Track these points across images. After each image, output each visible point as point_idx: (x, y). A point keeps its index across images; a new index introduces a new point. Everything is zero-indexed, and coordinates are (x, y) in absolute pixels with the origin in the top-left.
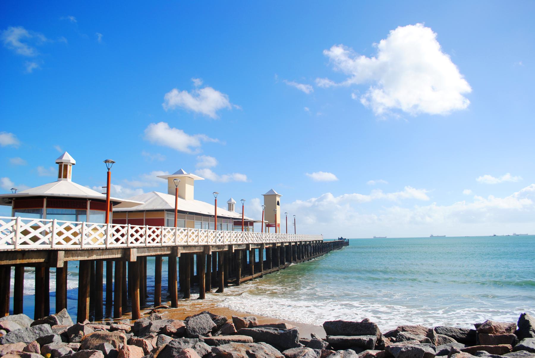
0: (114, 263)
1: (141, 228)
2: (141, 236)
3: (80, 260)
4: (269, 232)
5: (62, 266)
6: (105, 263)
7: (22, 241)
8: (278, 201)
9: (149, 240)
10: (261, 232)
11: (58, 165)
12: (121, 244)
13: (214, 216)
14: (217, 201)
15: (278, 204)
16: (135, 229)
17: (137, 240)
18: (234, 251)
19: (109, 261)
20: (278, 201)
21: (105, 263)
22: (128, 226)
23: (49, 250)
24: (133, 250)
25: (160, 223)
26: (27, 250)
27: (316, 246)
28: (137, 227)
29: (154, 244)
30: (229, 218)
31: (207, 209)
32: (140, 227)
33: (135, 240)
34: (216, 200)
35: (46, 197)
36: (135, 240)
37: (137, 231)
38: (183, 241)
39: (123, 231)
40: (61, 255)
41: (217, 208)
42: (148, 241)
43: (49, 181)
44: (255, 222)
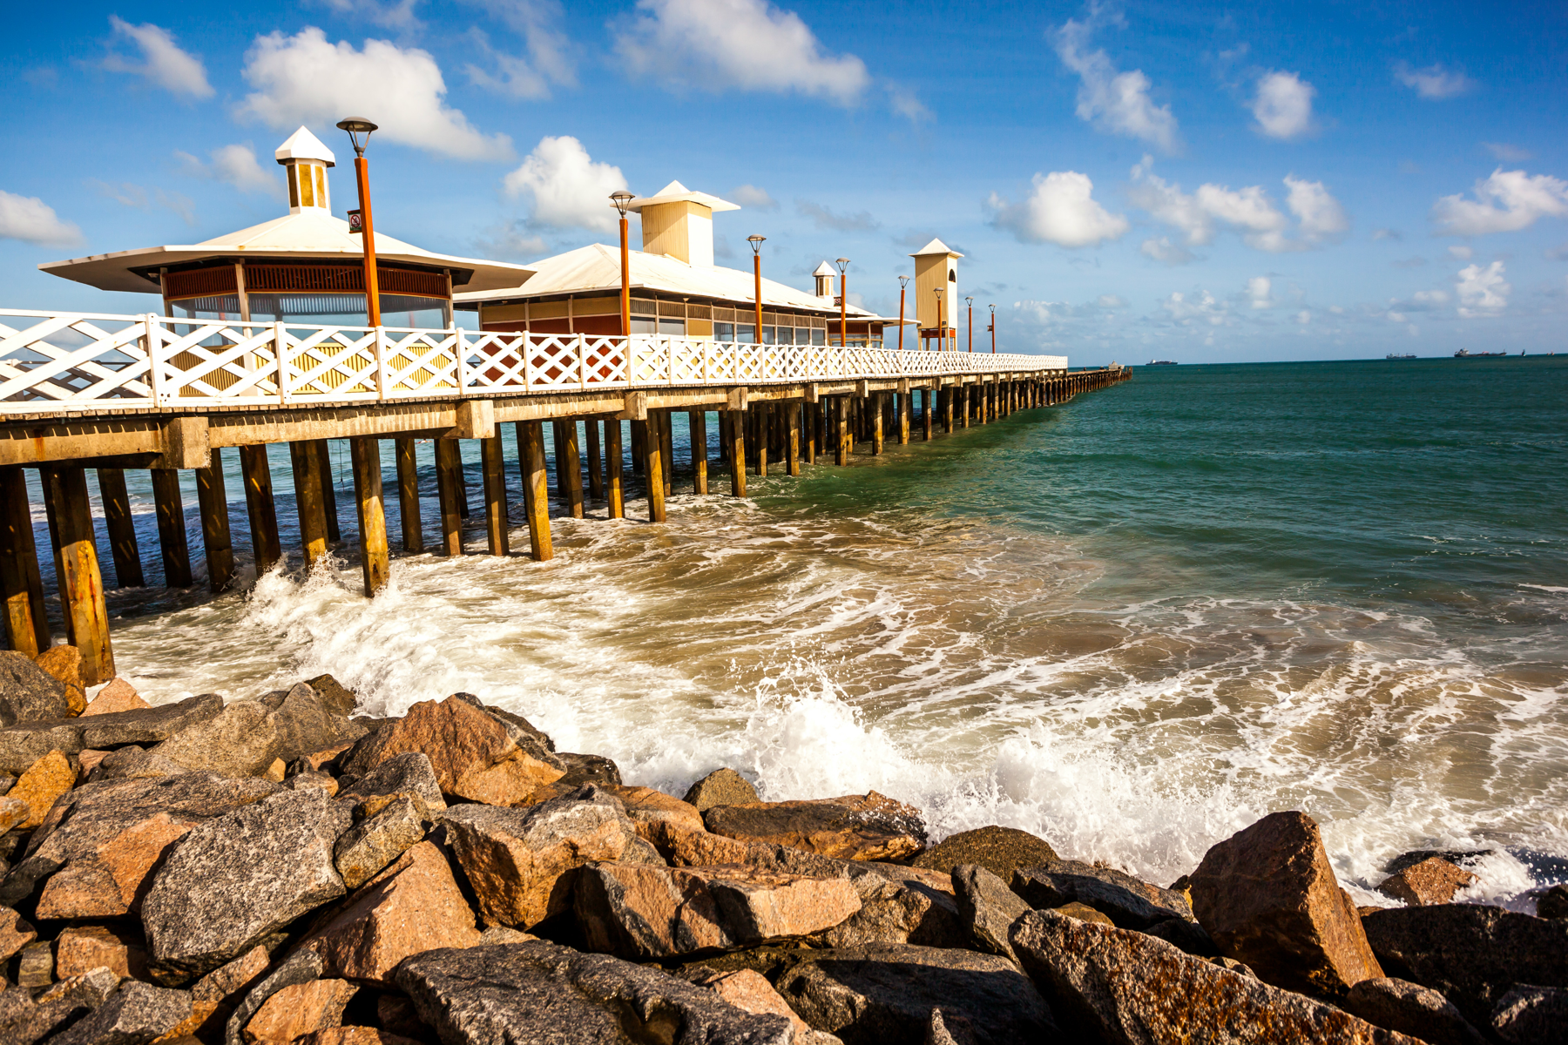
0: (601, 423)
1: (566, 341)
2: (567, 361)
3: (292, 444)
4: (661, 321)
5: (206, 463)
6: (580, 426)
7: (471, 380)
8: (952, 272)
9: (594, 371)
10: (652, 323)
11: (284, 168)
12: (506, 384)
13: (751, 306)
14: (761, 263)
15: (952, 277)
16: (598, 345)
17: (554, 373)
18: (867, 395)
19: (591, 419)
20: (952, 272)
21: (580, 426)
22: (580, 339)
23: (149, 414)
24: (479, 407)
25: (614, 326)
26: (37, 418)
27: (1048, 384)
28: (552, 339)
29: (556, 385)
30: (812, 313)
31: (736, 286)
32: (611, 340)
33: (600, 372)
34: (756, 259)
35: (243, 260)
36: (600, 372)
37: (552, 350)
38: (656, 374)
39: (566, 350)
40: (193, 430)
41: (762, 280)
42: (586, 374)
43: (265, 214)
44: (886, 323)
